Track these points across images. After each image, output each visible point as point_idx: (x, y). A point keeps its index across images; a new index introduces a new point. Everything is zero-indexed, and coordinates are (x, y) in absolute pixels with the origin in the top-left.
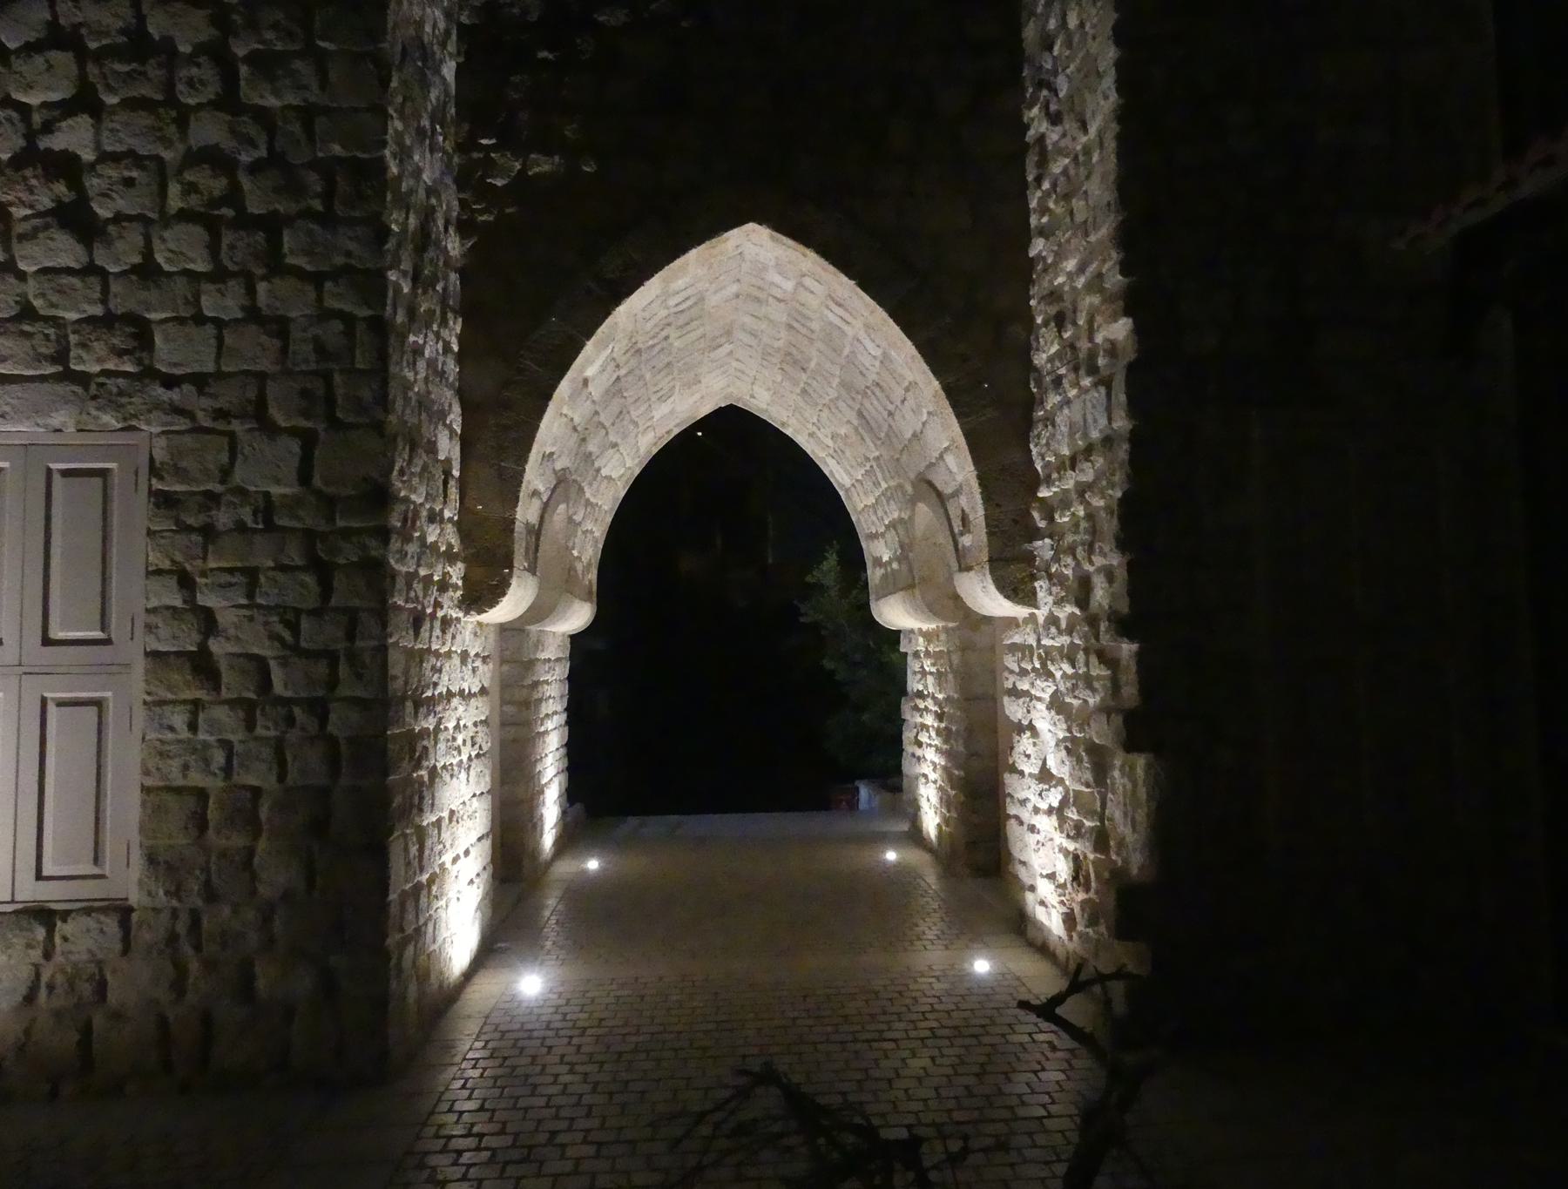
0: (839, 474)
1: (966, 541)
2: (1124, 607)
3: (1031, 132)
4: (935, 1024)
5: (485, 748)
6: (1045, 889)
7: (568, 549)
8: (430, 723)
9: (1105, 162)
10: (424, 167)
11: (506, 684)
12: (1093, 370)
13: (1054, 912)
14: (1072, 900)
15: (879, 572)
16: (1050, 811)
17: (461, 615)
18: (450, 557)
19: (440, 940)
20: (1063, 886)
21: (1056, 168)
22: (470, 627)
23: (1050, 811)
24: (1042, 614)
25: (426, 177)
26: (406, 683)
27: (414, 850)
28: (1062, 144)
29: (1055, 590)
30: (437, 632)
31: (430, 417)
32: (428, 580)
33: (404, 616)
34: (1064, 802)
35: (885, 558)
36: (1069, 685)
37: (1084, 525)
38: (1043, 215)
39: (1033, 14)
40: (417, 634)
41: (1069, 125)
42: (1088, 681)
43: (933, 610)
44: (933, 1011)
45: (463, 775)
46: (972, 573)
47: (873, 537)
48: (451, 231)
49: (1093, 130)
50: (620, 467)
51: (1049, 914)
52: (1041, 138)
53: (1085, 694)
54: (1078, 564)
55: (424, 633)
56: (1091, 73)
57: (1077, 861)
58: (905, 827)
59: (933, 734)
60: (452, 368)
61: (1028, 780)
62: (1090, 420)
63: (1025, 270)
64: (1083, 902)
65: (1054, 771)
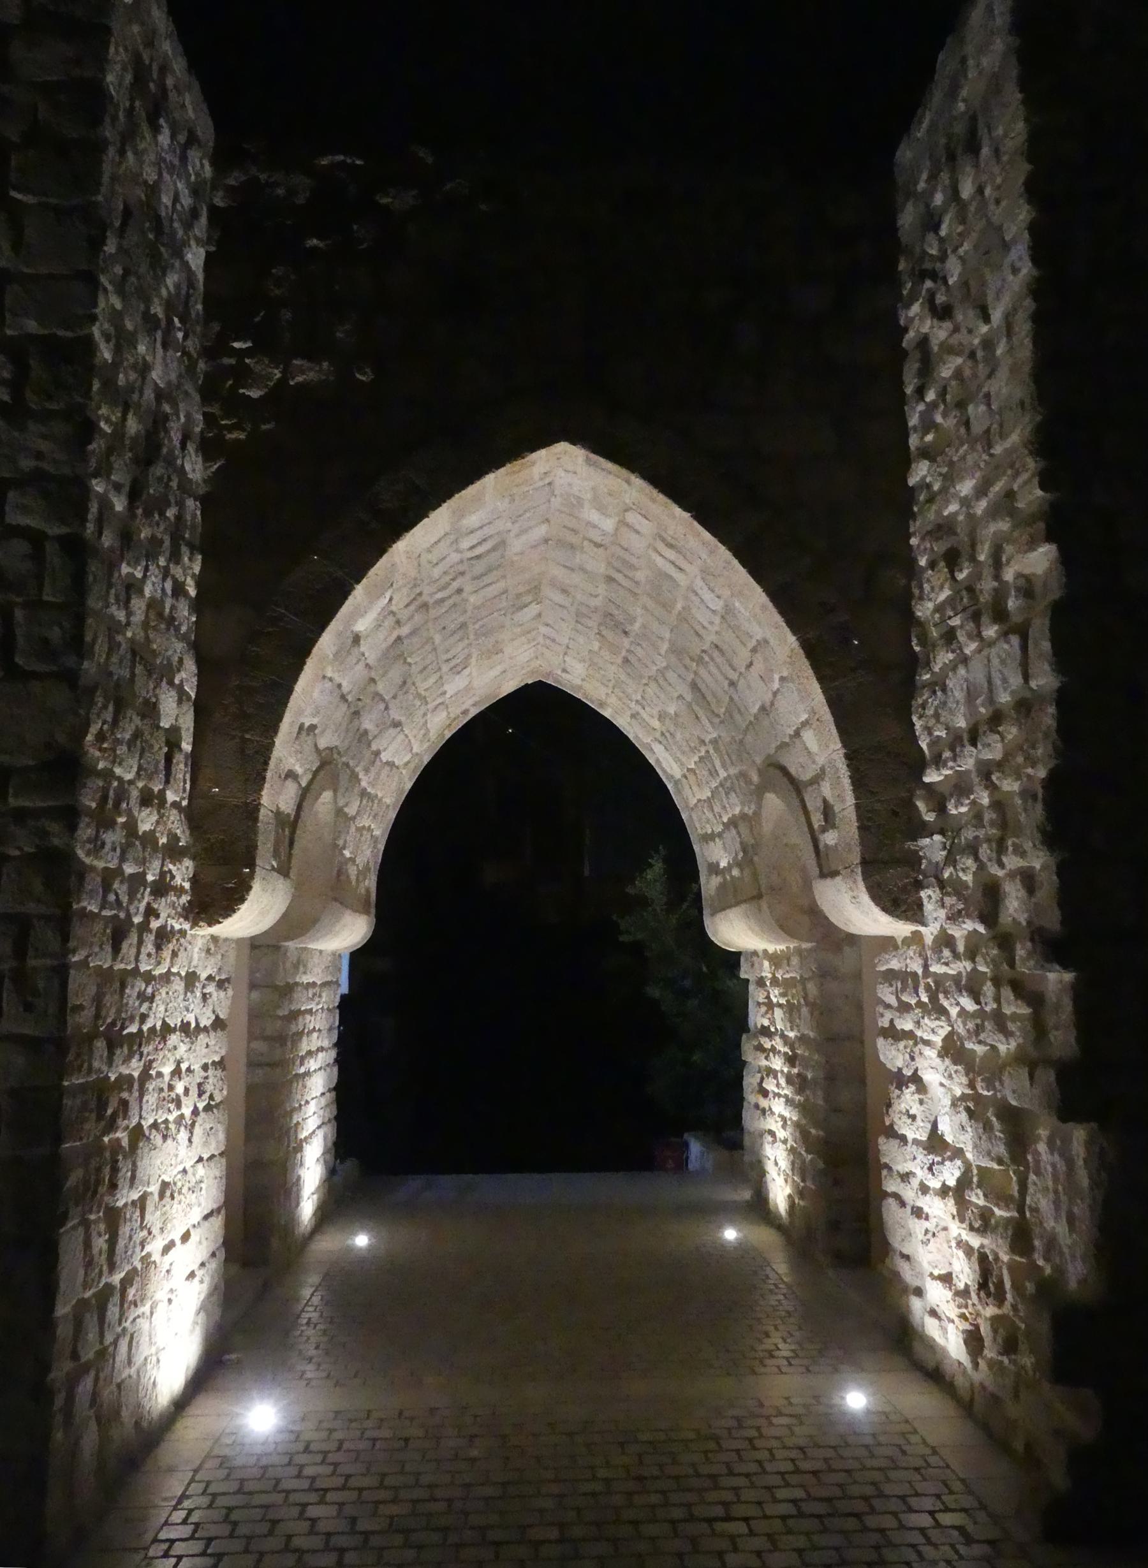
0: (667, 762)
1: (830, 838)
2: (1053, 921)
3: (911, 334)
4: (799, 1493)
5: (218, 1098)
6: (937, 1294)
7: (337, 849)
8: (134, 1068)
9: (1016, 352)
10: (154, 363)
11: (256, 1015)
12: (1000, 615)
13: (951, 1328)
14: (978, 1314)
15: (716, 881)
16: (944, 1191)
17: (186, 926)
18: (173, 852)
19: (138, 1360)
20: (964, 1293)
21: (946, 372)
22: (200, 943)
23: (944, 1191)
24: (929, 932)
25: (155, 375)
26: (97, 1016)
27: (100, 1243)
28: (954, 341)
29: (948, 901)
30: (149, 947)
31: (150, 673)
32: (137, 881)
33: (98, 927)
34: (964, 1183)
35: (723, 864)
36: (971, 1025)
37: (988, 816)
38: (926, 433)
39: (910, 194)
40: (116, 949)
41: (964, 315)
42: (1000, 1022)
43: (785, 927)
44: (797, 1471)
45: (183, 1135)
46: (838, 879)
47: (708, 838)
48: (191, 448)
49: (997, 316)
50: (404, 753)
51: (944, 1330)
52: (924, 342)
53: (991, 1036)
54: (981, 867)
55: (128, 947)
56: (994, 245)
57: (985, 1264)
58: (746, 1195)
59: (782, 1081)
60: (186, 616)
61: (911, 1149)
62: (998, 682)
63: (903, 503)
64: (995, 1321)
65: (949, 1139)
